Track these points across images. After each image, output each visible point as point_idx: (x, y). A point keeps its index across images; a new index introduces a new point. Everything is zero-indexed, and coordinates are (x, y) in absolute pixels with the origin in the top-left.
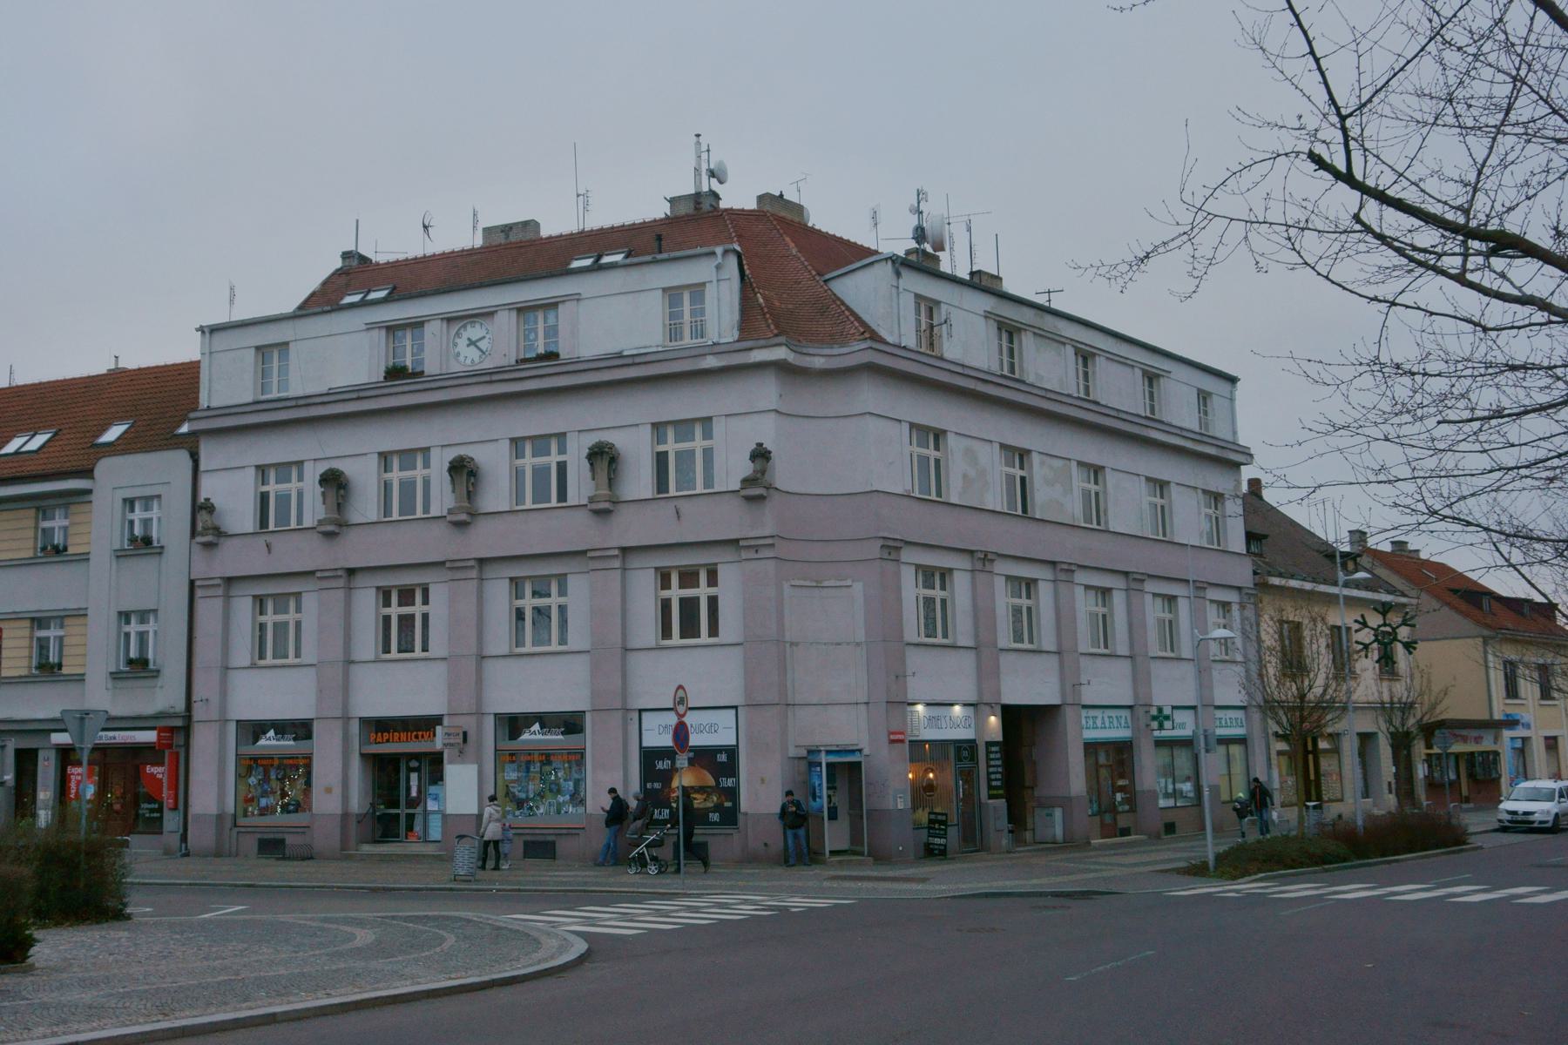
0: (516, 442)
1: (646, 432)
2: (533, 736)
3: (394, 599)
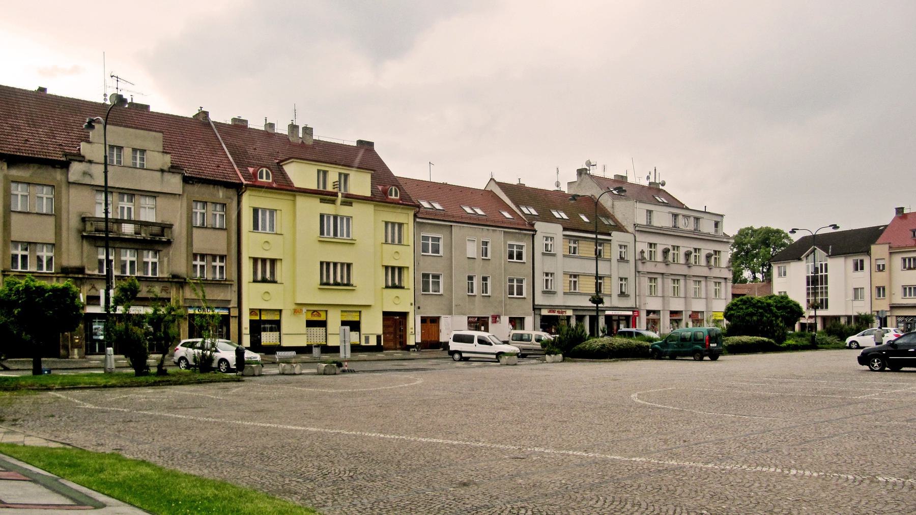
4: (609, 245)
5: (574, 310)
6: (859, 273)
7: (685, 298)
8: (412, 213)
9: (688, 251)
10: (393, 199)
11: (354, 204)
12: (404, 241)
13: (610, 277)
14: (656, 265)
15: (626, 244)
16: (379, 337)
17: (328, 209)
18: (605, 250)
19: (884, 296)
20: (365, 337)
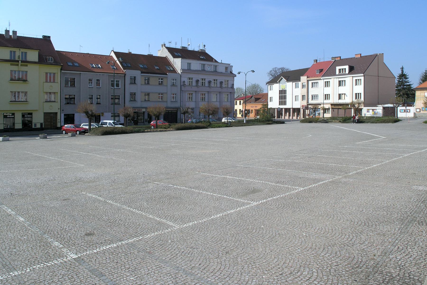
7: (196, 102)
8: (59, 68)
9: (209, 81)
10: (50, 62)
11: (28, 65)
12: (56, 81)
13: (166, 93)
14: (191, 88)
16: (41, 124)
17: (15, 68)
18: (165, 81)
20: (34, 124)
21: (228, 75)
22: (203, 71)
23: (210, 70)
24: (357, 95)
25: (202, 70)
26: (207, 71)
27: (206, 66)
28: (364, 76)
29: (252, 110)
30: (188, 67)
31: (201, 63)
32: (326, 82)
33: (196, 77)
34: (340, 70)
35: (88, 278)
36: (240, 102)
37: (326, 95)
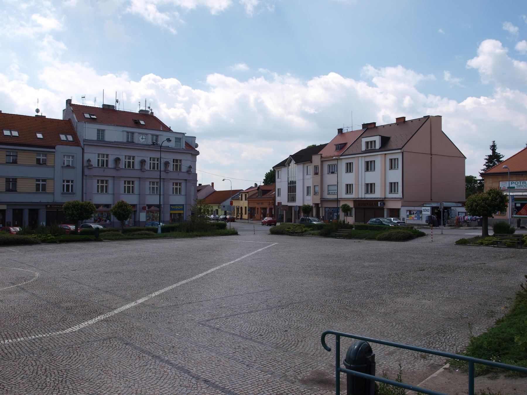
0: (99, 154)
1: (97, 155)
2: (153, 208)
3: (65, 181)
4: (53, 155)
5: (7, 205)
6: (349, 174)
15: (73, 155)
19: (352, 192)
21: (181, 151)
22: (130, 144)
23: (145, 143)
24: (393, 186)
25: (128, 141)
26: (137, 144)
27: (136, 135)
28: (403, 153)
29: (258, 208)
30: (98, 136)
31: (125, 131)
32: (347, 164)
33: (113, 154)
34: (367, 143)
35: (249, 387)
36: (292, 198)
37: (367, 184)
